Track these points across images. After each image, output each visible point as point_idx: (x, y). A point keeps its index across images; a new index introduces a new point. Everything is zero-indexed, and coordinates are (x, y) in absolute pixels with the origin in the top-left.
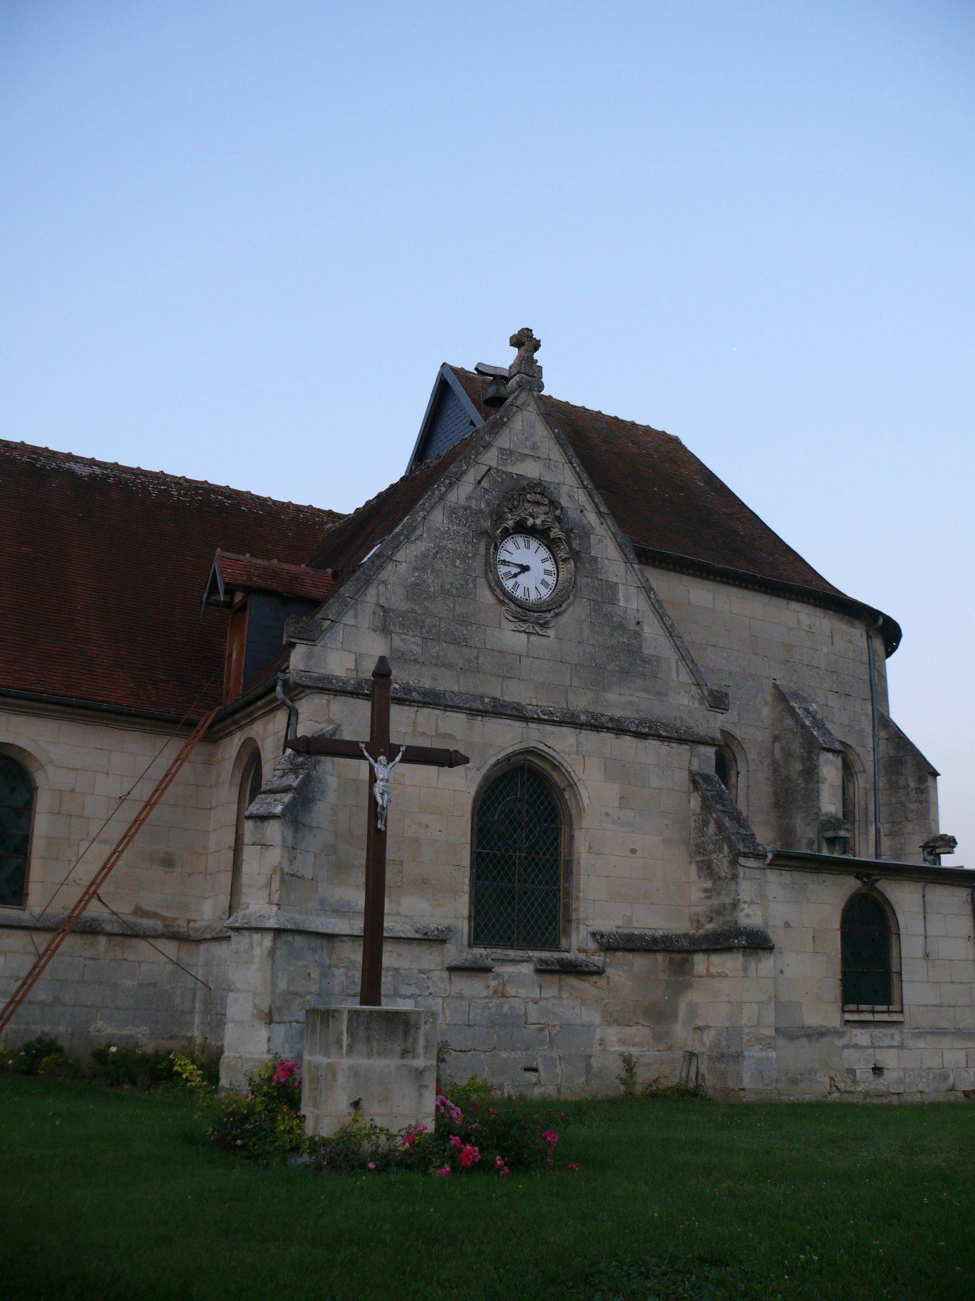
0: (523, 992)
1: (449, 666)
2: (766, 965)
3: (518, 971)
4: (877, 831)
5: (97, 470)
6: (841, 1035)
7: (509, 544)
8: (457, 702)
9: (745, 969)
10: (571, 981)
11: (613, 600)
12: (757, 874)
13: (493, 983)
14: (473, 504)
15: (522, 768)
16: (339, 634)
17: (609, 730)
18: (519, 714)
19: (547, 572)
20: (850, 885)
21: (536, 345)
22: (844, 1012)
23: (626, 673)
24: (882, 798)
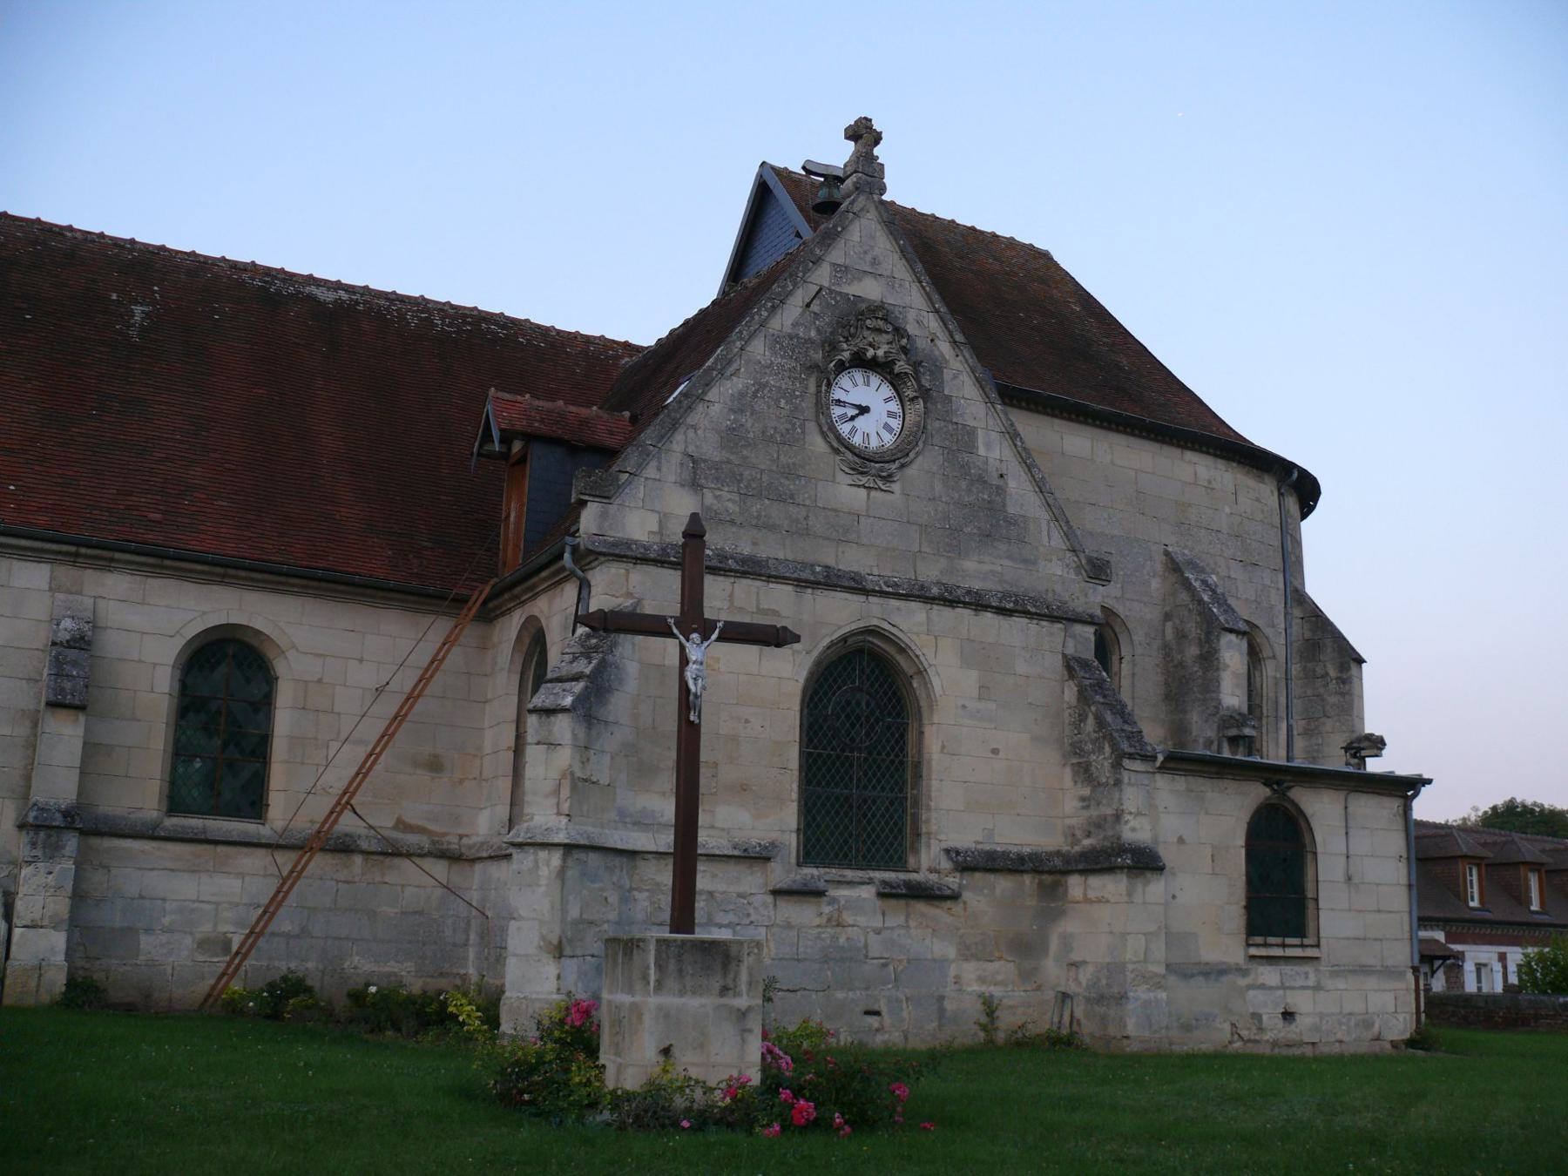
0: (862, 920)
1: (772, 528)
2: (1155, 888)
3: (856, 894)
4: (1290, 729)
7: (844, 380)
8: (782, 571)
10: (921, 907)
11: (971, 448)
12: (1145, 779)
13: (827, 910)
14: (801, 332)
16: (639, 490)
17: (966, 605)
18: (857, 586)
19: (891, 414)
20: (1258, 793)
22: (1249, 945)
23: (987, 537)
24: (1296, 689)
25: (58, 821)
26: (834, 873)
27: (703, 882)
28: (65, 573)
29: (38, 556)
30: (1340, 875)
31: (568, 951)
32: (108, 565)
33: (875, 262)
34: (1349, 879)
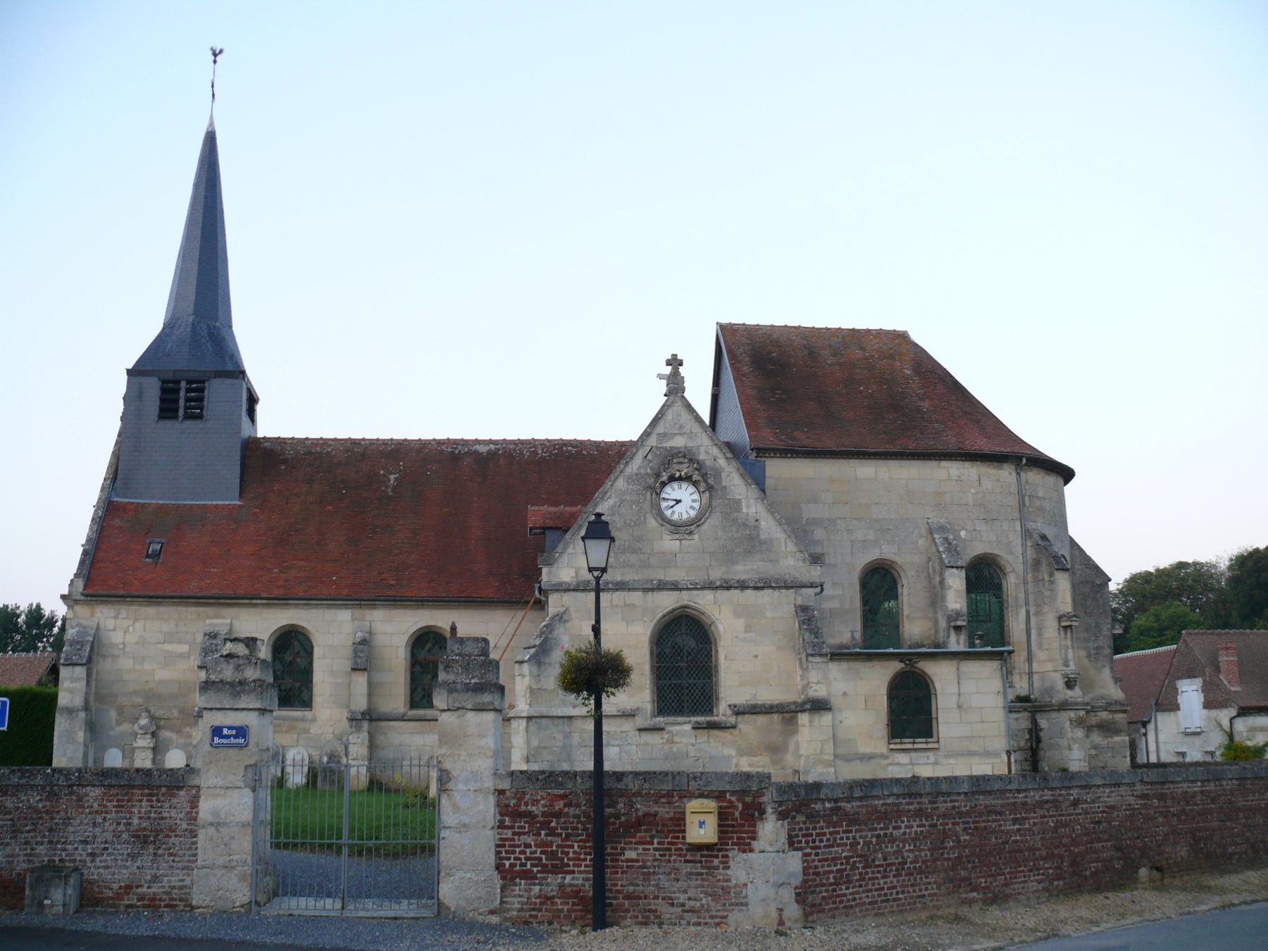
0: (684, 740)
1: (631, 566)
2: (826, 719)
3: (682, 729)
4: (1028, 613)
5: (492, 447)
6: (886, 757)
7: (668, 489)
8: (636, 585)
9: (810, 722)
10: (716, 732)
11: (739, 509)
12: (822, 666)
13: (666, 736)
14: (642, 471)
15: (681, 617)
16: (565, 559)
17: (736, 588)
18: (675, 587)
19: (694, 501)
20: (895, 666)
21: (681, 364)
23: (748, 552)
24: (1031, 588)
25: (360, 717)
26: (671, 719)
27: (605, 728)
28: (358, 612)
29: (346, 607)
30: (953, 702)
31: (532, 759)
32: (374, 607)
33: (681, 427)
34: (959, 707)
